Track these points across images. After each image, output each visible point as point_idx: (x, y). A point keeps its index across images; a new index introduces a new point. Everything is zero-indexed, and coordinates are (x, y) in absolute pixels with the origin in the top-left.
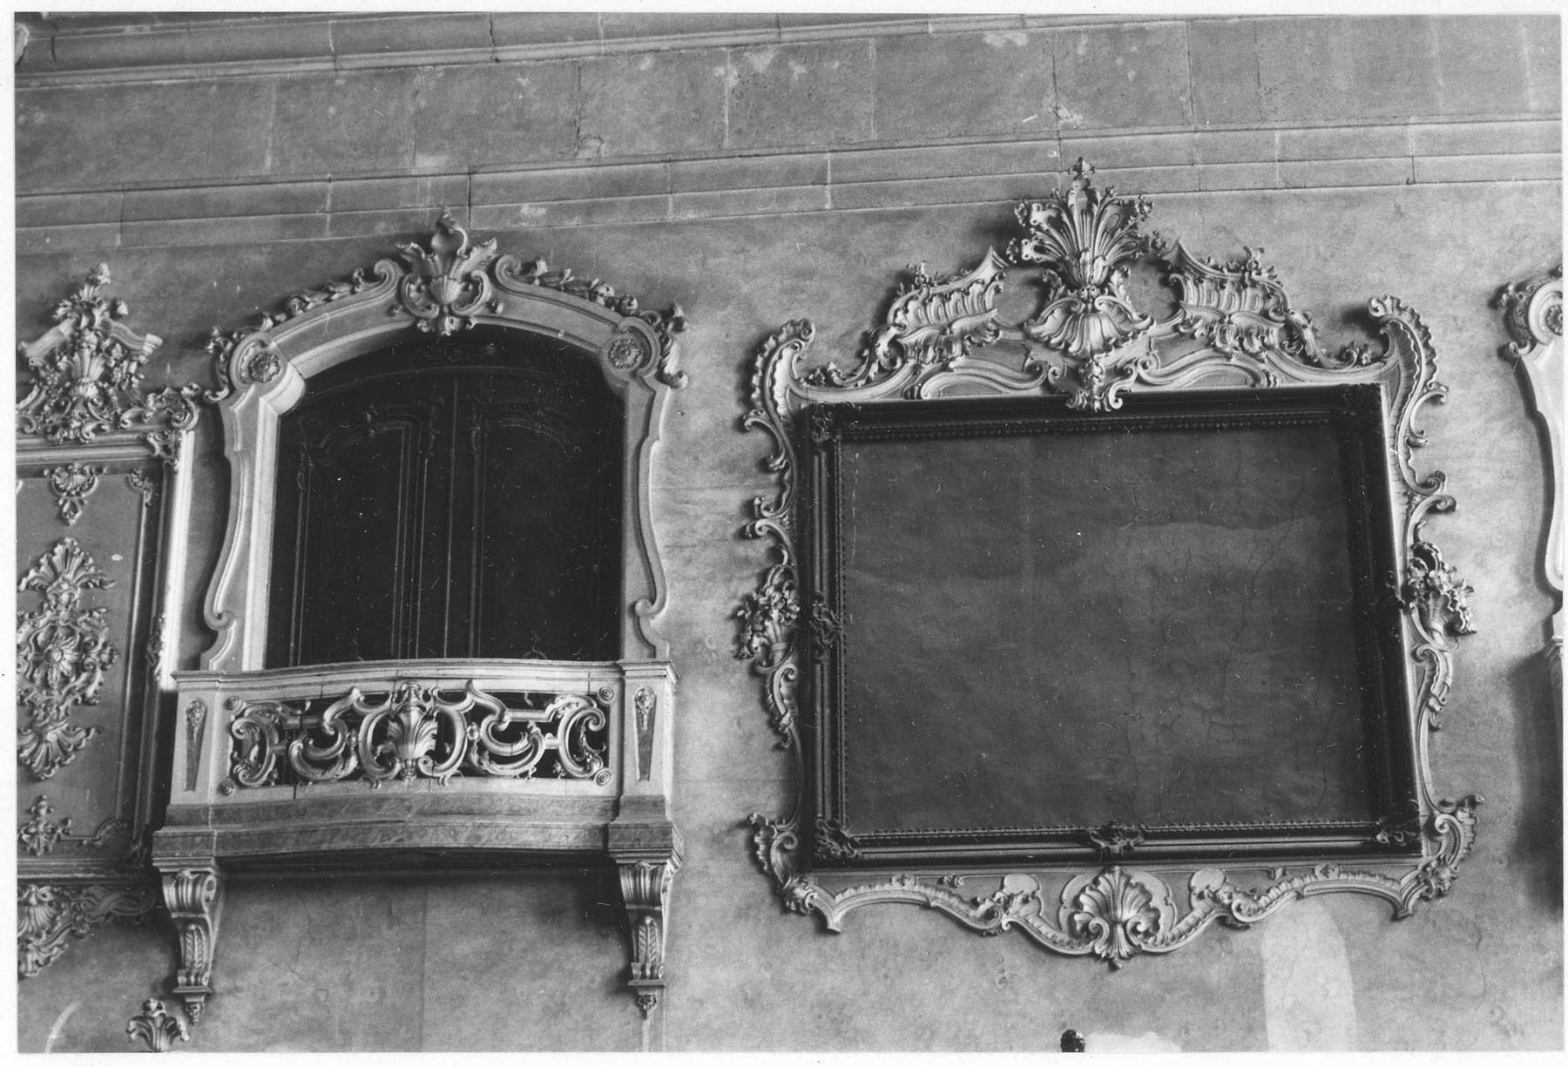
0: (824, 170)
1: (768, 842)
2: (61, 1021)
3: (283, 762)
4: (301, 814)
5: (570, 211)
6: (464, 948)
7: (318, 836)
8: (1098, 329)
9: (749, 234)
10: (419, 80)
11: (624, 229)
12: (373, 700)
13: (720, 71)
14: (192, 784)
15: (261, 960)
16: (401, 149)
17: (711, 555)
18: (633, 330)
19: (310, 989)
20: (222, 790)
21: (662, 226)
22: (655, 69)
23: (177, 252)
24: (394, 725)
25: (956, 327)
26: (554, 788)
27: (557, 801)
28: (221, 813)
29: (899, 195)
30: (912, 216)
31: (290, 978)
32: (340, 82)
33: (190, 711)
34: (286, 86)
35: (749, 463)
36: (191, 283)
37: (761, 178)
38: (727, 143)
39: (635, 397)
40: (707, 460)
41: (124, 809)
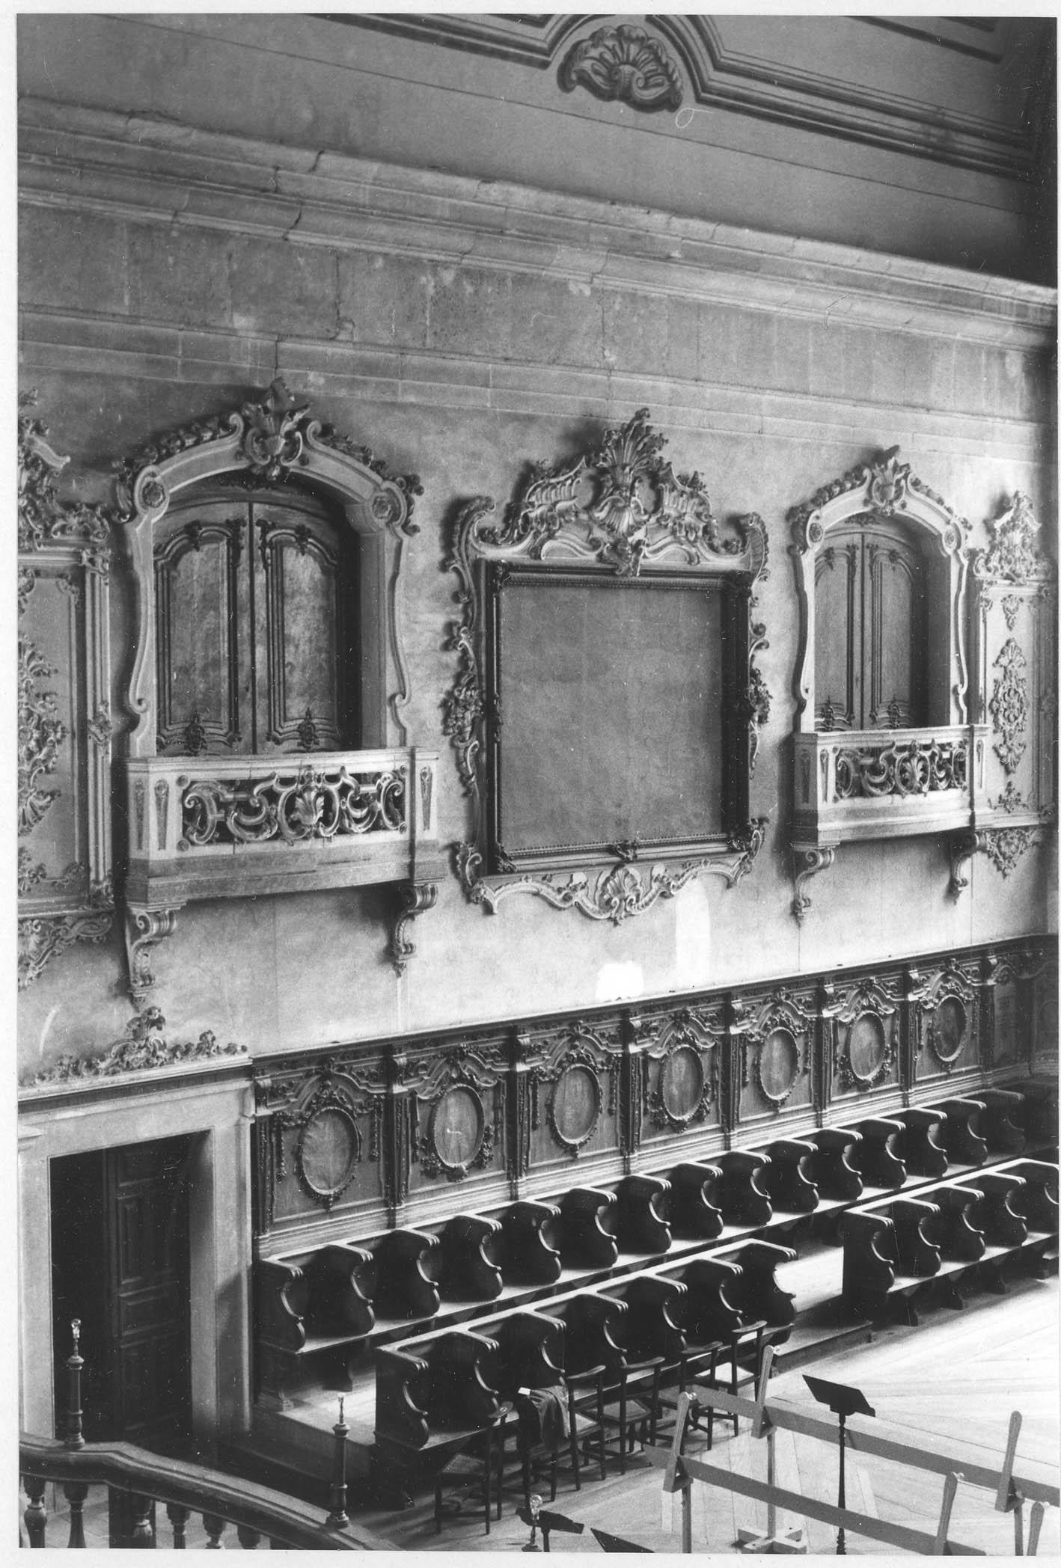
0: (487, 376)
1: (464, 859)
2: (49, 1020)
3: (221, 827)
4: (243, 865)
5: (339, 383)
6: (300, 939)
7: (262, 883)
8: (627, 519)
9: (446, 419)
10: (231, 245)
11: (373, 403)
12: (286, 782)
13: (424, 279)
14: (162, 845)
15: (178, 961)
16: (222, 306)
17: (431, 661)
18: (389, 490)
19: (208, 979)
20: (181, 846)
21: (393, 404)
22: (385, 268)
23: (69, 376)
24: (299, 801)
25: (559, 506)
26: (379, 837)
27: (383, 846)
28: (181, 865)
29: (526, 400)
30: (530, 419)
31: (195, 971)
32: (175, 234)
33: (158, 788)
34: (135, 228)
35: (447, 595)
36: (83, 407)
37: (452, 375)
38: (428, 341)
39: (389, 541)
40: (427, 591)
41: (81, 856)
